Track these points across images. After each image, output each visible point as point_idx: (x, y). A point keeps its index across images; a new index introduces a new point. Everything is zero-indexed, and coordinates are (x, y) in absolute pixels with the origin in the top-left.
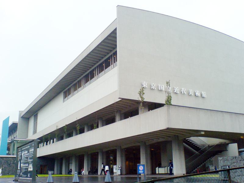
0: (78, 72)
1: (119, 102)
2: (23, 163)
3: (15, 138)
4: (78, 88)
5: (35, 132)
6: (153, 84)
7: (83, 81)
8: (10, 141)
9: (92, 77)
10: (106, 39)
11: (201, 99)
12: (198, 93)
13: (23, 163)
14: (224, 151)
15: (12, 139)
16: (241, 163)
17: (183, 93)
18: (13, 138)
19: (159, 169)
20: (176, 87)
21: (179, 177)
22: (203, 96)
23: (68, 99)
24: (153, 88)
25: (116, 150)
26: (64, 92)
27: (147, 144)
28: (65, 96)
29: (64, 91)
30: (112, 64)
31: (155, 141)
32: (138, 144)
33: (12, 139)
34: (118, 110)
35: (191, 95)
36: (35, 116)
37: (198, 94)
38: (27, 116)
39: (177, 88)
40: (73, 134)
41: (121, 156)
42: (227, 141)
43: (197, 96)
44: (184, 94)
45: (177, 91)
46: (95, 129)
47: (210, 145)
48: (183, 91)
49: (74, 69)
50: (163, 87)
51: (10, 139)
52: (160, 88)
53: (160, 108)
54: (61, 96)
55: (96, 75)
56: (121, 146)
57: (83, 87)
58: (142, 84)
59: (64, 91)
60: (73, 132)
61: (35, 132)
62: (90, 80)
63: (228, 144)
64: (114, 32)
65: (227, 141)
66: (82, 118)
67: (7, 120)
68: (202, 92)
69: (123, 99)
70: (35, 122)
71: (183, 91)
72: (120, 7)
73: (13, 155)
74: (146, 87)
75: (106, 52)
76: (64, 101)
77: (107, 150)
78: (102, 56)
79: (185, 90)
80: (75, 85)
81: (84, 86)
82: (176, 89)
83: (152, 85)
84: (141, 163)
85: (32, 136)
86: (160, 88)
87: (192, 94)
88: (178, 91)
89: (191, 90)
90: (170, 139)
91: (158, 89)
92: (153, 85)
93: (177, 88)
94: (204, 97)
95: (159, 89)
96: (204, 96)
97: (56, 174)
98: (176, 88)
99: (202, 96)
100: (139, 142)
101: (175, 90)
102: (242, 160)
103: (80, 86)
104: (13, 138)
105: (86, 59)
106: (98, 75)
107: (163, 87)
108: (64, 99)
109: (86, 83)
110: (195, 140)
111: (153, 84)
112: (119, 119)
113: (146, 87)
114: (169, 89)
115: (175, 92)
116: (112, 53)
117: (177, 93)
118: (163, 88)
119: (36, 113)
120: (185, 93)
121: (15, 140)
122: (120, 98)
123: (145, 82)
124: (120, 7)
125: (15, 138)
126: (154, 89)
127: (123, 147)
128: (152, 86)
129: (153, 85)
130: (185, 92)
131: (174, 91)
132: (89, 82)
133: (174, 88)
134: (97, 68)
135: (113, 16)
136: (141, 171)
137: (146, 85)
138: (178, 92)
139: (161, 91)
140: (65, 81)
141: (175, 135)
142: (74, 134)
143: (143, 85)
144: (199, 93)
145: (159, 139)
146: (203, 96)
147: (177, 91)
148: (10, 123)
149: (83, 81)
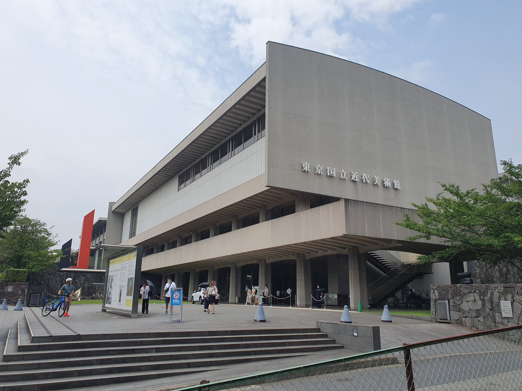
0: (205, 144)
1: (213, 214)
3: (101, 242)
4: (202, 170)
5: (132, 234)
8: (93, 247)
9: (224, 154)
10: (243, 99)
11: (392, 192)
14: (427, 273)
15: (97, 244)
16: (470, 296)
17: (364, 181)
18: (97, 242)
22: (395, 187)
23: (201, 176)
27: (307, 258)
28: (181, 183)
29: (180, 174)
30: (255, 135)
31: (320, 254)
33: (97, 244)
34: (263, 204)
35: (377, 185)
36: (133, 211)
37: (387, 183)
38: (121, 211)
39: (357, 173)
40: (191, 238)
41: (266, 275)
43: (386, 187)
44: (366, 183)
46: (155, 253)
47: (405, 264)
48: (365, 178)
50: (335, 171)
51: (94, 244)
52: (330, 172)
53: (334, 204)
54: (175, 182)
56: (236, 264)
58: (302, 166)
59: (180, 174)
60: (191, 236)
61: (132, 234)
67: (91, 215)
69: (272, 187)
70: (133, 219)
71: (365, 178)
72: (271, 45)
73: (97, 269)
74: (308, 170)
75: (246, 116)
76: (179, 190)
77: (199, 270)
78: (239, 122)
81: (210, 168)
82: (355, 175)
83: (317, 167)
86: (330, 172)
88: (357, 178)
90: (344, 252)
92: (319, 168)
93: (357, 173)
94: (396, 189)
95: (328, 174)
97: (304, 303)
98: (355, 174)
99: (394, 186)
100: (230, 264)
103: (204, 167)
104: (97, 242)
105: (217, 126)
106: (259, 132)
107: (335, 171)
108: (179, 186)
109: (214, 162)
110: (383, 255)
111: (319, 165)
112: (195, 239)
113: (308, 170)
114: (343, 175)
115: (352, 179)
116: (255, 118)
117: (355, 181)
119: (135, 206)
120: (368, 181)
121: (103, 246)
122: (267, 186)
123: (306, 163)
124: (271, 45)
125: (101, 242)
126: (320, 174)
127: (268, 261)
128: (317, 169)
129: (319, 168)
131: (351, 177)
134: (194, 167)
137: (309, 168)
139: (331, 177)
140: (196, 148)
142: (261, 219)
143: (304, 167)
145: (326, 251)
146: (395, 187)
148: (95, 220)
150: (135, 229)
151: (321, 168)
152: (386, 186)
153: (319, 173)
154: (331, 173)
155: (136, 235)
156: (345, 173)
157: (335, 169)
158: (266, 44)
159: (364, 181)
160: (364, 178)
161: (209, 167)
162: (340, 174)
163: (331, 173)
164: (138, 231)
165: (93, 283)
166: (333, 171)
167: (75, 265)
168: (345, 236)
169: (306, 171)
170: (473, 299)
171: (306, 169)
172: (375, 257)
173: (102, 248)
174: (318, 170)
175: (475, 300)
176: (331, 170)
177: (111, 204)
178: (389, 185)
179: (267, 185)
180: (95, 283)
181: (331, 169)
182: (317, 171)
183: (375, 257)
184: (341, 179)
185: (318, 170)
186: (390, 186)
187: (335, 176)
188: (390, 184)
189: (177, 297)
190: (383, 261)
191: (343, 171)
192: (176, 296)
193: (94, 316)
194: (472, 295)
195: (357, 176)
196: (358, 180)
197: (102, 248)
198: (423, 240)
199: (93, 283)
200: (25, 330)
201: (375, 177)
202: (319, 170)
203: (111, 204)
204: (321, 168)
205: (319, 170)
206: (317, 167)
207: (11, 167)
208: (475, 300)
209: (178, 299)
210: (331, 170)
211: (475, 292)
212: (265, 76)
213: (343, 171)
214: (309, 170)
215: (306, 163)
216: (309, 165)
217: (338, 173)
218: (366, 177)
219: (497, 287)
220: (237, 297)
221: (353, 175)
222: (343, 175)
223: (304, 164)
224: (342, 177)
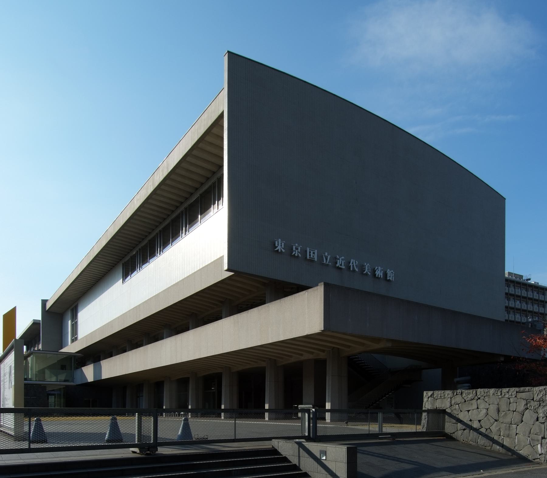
12: (379, 272)
16: (472, 404)
17: (351, 269)
19: (144, 418)
22: (388, 279)
24: (296, 255)
25: (189, 378)
26: (123, 264)
28: (126, 275)
32: (263, 364)
35: (367, 274)
36: (72, 310)
39: (343, 258)
44: (354, 271)
45: (341, 265)
48: (353, 265)
49: (108, 246)
52: (310, 255)
54: (120, 272)
58: (275, 245)
68: (388, 270)
71: (353, 265)
72: (42, 300)
80: (166, 229)
83: (294, 247)
86: (310, 255)
87: (369, 274)
88: (343, 265)
89: (368, 264)
91: (306, 258)
92: (297, 249)
93: (343, 258)
95: (308, 257)
96: (391, 279)
102: (476, 398)
113: (281, 251)
115: (337, 265)
120: (357, 270)
123: (280, 240)
124: (42, 300)
128: (294, 249)
129: (297, 249)
130: (355, 268)
131: (336, 263)
133: (336, 258)
141: (334, 347)
143: (276, 245)
144: (382, 272)
145: (302, 355)
146: (388, 279)
147: (341, 265)
151: (299, 248)
152: (377, 276)
157: (316, 251)
163: (312, 257)
169: (280, 251)
170: (476, 407)
175: (478, 408)
182: (294, 253)
185: (295, 251)
188: (382, 275)
191: (326, 254)
194: (474, 402)
196: (344, 267)
204: (299, 248)
208: (478, 408)
211: (479, 398)
216: (283, 244)
219: (508, 392)
221: (338, 261)
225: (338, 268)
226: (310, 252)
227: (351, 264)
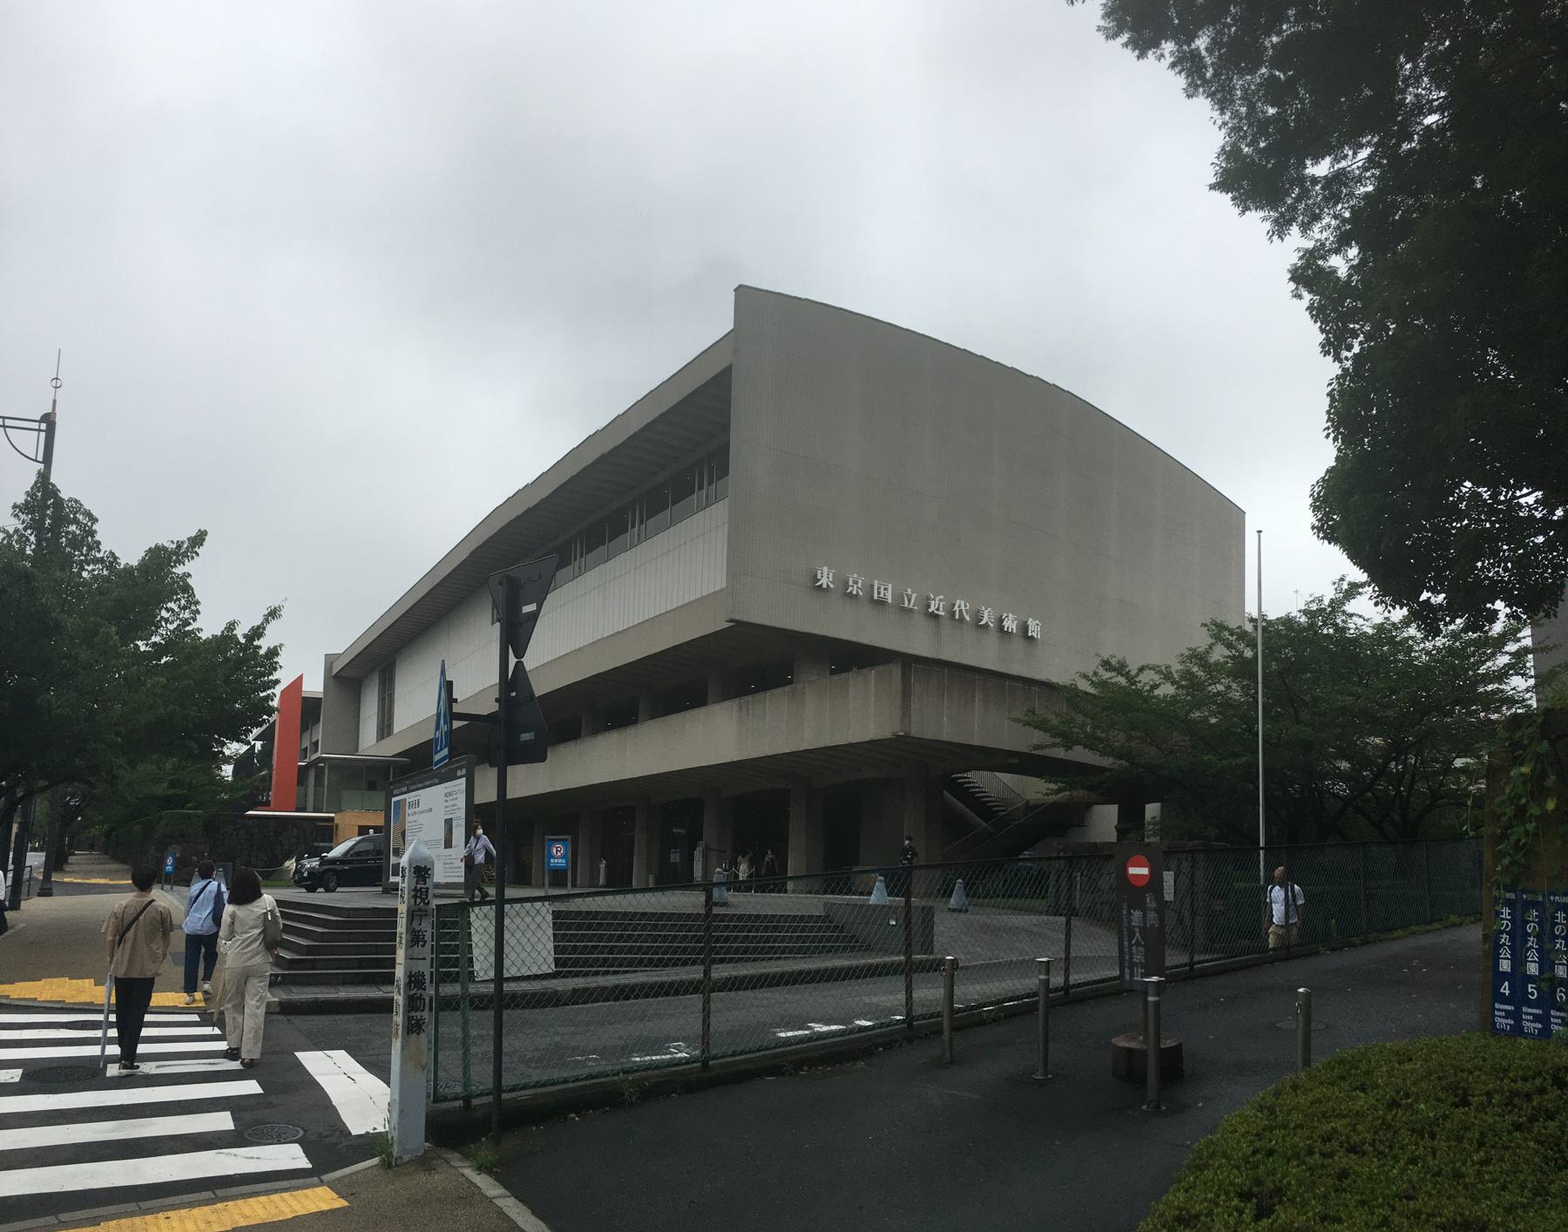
2: (908, 953)
5: (385, 729)
6: (855, 576)
7: (578, 546)
11: (1018, 645)
12: (1010, 621)
13: (908, 953)
17: (957, 617)
20: (936, 596)
21: (515, 899)
22: (1030, 634)
37: (1010, 624)
39: (941, 597)
42: (1080, 793)
43: (1007, 632)
44: (962, 619)
52: (879, 593)
55: (578, 558)
57: (577, 570)
61: (385, 729)
62: (609, 541)
63: (1089, 806)
64: (731, 365)
65: (1080, 793)
66: (687, 643)
71: (961, 611)
74: (828, 585)
79: (966, 606)
82: (937, 602)
84: (789, 875)
85: (370, 744)
86: (879, 593)
88: (941, 609)
92: (856, 582)
93: (941, 597)
95: (876, 598)
98: (937, 599)
101: (932, 605)
106: (641, 522)
113: (828, 585)
114: (909, 600)
115: (930, 610)
117: (937, 616)
118: (890, 595)
120: (968, 618)
123: (825, 568)
128: (851, 583)
131: (929, 606)
132: (309, 731)
133: (928, 598)
135: (719, 322)
136: (556, 860)
137: (831, 579)
138: (941, 613)
139: (881, 603)
143: (819, 577)
146: (1030, 634)
149: (578, 546)
150: (391, 718)
151: (860, 581)
152: (1006, 629)
153: (854, 592)
154: (882, 595)
155: (395, 732)
156: (914, 596)
157: (890, 585)
158: (735, 290)
159: (957, 617)
160: (958, 609)
161: (577, 561)
162: (903, 599)
163: (882, 595)
164: (398, 727)
165: (316, 844)
166: (885, 589)
167: (266, 805)
168: (897, 739)
169: (825, 586)
171: (824, 582)
172: (974, 790)
173: (322, 765)
174: (853, 586)
176: (882, 588)
177: (330, 660)
178: (1012, 629)
179: (728, 618)
180: (321, 844)
181: (883, 585)
183: (974, 790)
184: (903, 610)
185: (853, 586)
186: (1014, 631)
187: (890, 601)
188: (1014, 627)
189: (559, 854)
190: (977, 790)
191: (909, 591)
192: (557, 851)
193: (377, 895)
195: (941, 603)
196: (943, 614)
197: (322, 765)
198: (1060, 753)
199: (316, 844)
200: (978, 704)
201: (983, 608)
202: (855, 586)
203: (330, 660)
204: (860, 581)
205: (855, 586)
206: (851, 579)
207: (267, 621)
209: (562, 858)
210: (882, 588)
212: (731, 365)
213: (909, 591)
214: (832, 586)
215: (825, 568)
216: (831, 574)
217: (899, 598)
218: (963, 607)
220: (651, 877)
222: (909, 600)
223: (819, 572)
224: (906, 605)
225: (935, 616)
226: (879, 588)
227: (956, 608)
